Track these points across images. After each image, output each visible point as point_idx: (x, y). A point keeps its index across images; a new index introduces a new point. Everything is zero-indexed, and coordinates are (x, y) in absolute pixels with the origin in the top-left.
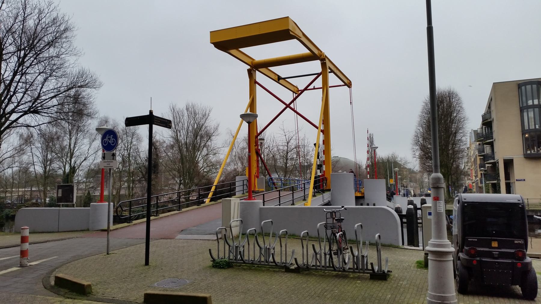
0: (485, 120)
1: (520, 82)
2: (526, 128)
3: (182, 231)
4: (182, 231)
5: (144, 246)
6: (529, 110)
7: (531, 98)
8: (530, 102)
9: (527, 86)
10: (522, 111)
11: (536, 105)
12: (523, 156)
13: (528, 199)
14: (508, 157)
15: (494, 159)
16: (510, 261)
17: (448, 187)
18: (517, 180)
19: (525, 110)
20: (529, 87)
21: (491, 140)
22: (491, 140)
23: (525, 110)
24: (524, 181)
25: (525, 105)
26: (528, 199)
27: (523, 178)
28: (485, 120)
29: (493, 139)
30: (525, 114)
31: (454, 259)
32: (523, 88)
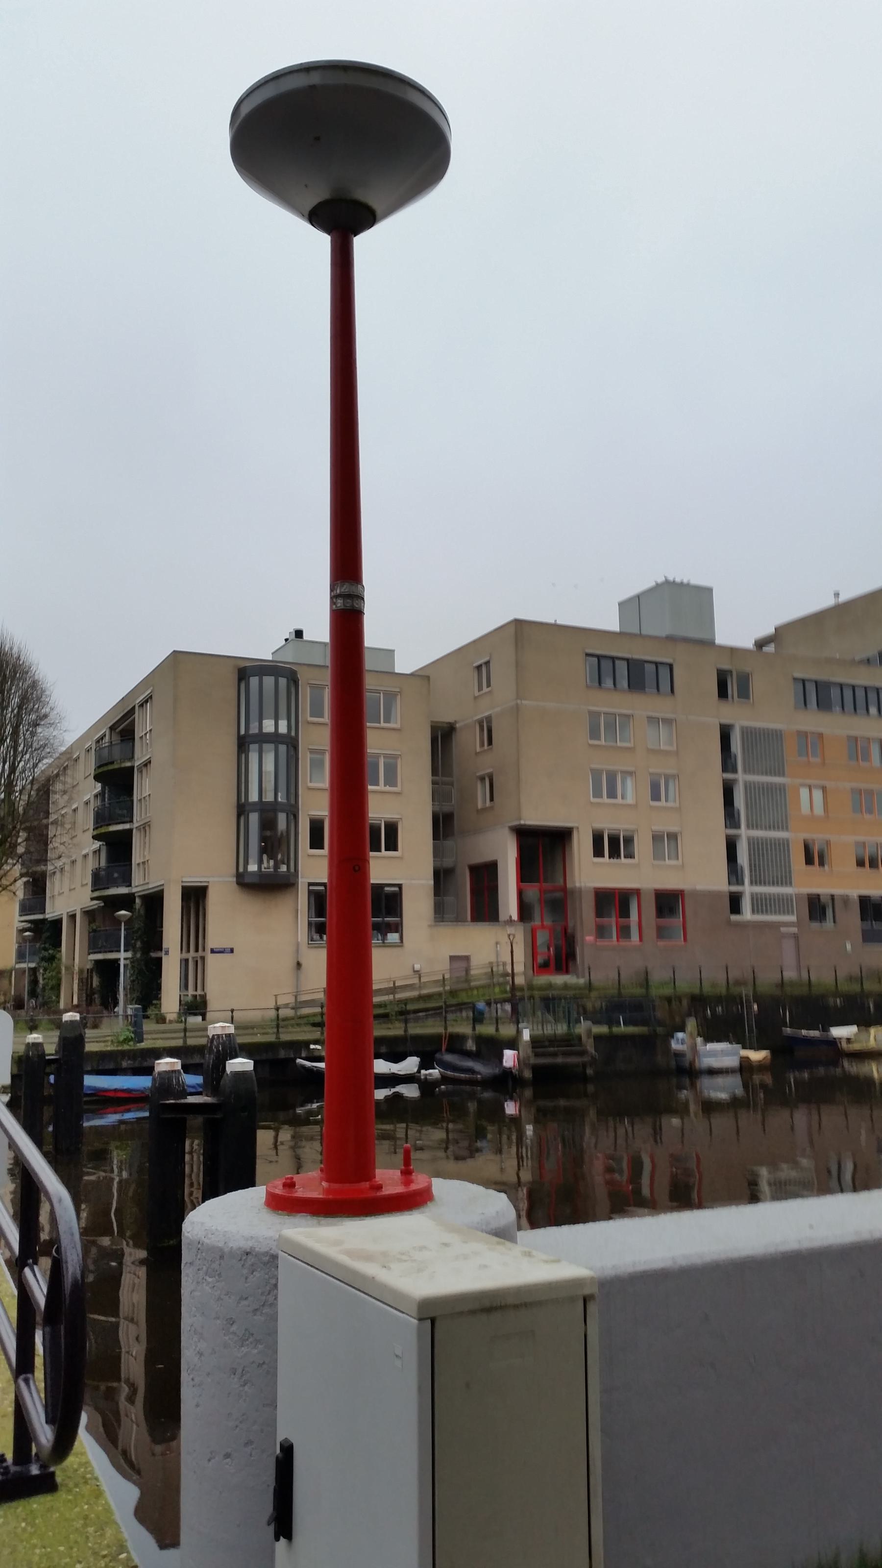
0: (106, 764)
1: (248, 664)
2: (254, 797)
3: (299, 965)
4: (299, 965)
5: (515, 961)
6: (266, 746)
7: (273, 715)
8: (268, 726)
9: (264, 677)
10: (243, 744)
11: (282, 735)
12: (235, 879)
13: (232, 1011)
14: (195, 879)
15: (130, 885)
16: (804, 1032)
17: (74, 966)
18: (213, 951)
19: (254, 747)
20: (269, 681)
21: (127, 826)
22: (127, 826)
23: (252, 747)
24: (231, 954)
25: (254, 730)
26: (232, 1011)
27: (227, 945)
28: (106, 764)
29: (131, 821)
30: (254, 757)
31: (322, 1150)
32: (254, 681)
